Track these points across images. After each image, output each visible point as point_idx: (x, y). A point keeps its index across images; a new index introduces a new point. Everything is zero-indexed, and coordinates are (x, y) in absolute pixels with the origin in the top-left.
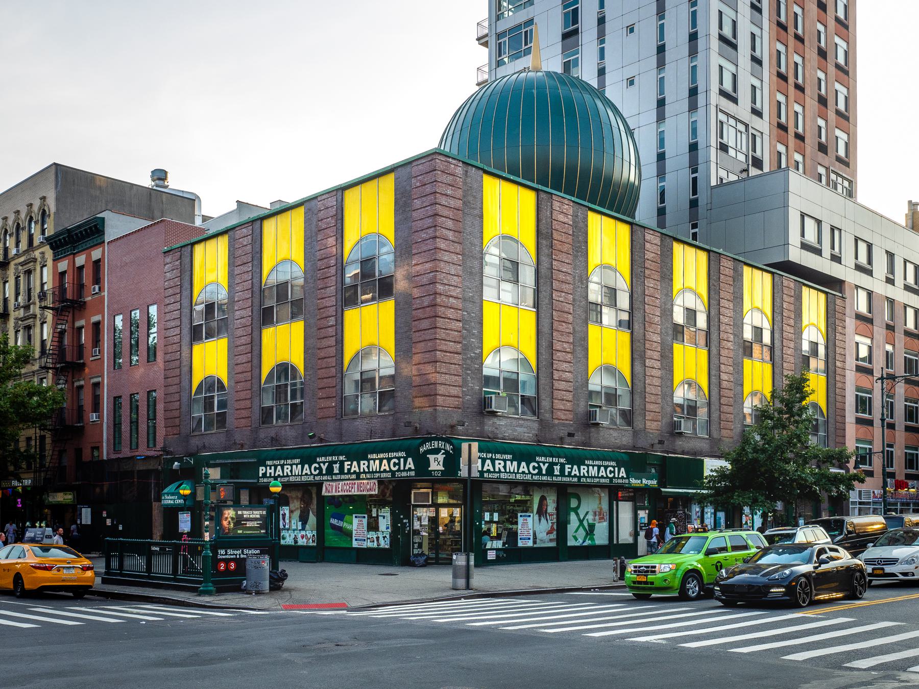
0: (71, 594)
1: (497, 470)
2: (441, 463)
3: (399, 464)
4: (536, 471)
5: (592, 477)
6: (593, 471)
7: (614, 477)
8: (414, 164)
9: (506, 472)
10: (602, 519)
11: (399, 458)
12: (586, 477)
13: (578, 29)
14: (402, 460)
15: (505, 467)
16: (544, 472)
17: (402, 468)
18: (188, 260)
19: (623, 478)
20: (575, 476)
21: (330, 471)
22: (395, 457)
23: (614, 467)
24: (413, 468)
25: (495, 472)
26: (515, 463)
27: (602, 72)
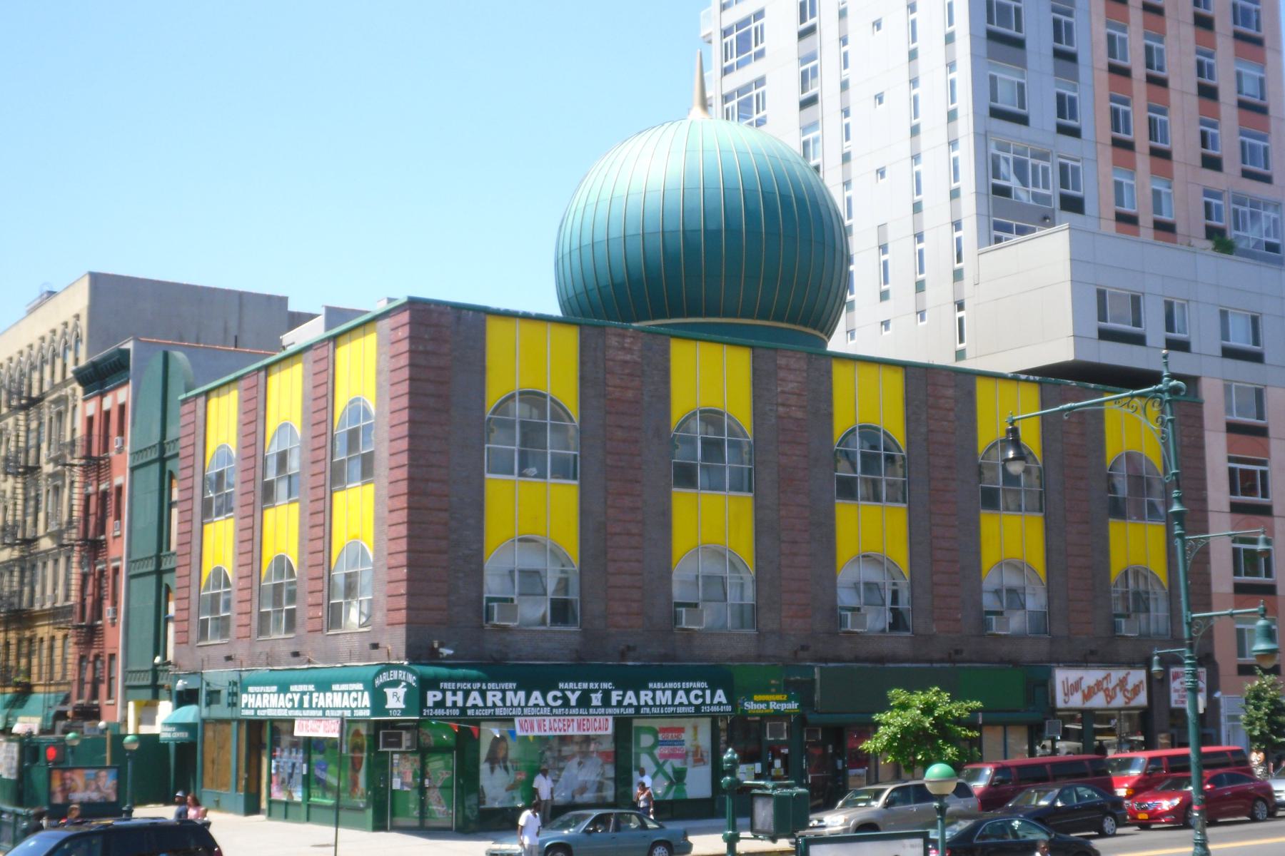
1: (489, 704)
2: (402, 699)
4: (559, 702)
5: (661, 706)
6: (664, 697)
7: (704, 703)
9: (505, 706)
10: (699, 760)
12: (651, 707)
15: (503, 700)
16: (573, 703)
18: (202, 431)
19: (720, 704)
20: (630, 705)
23: (703, 690)
25: (485, 707)
26: (522, 694)
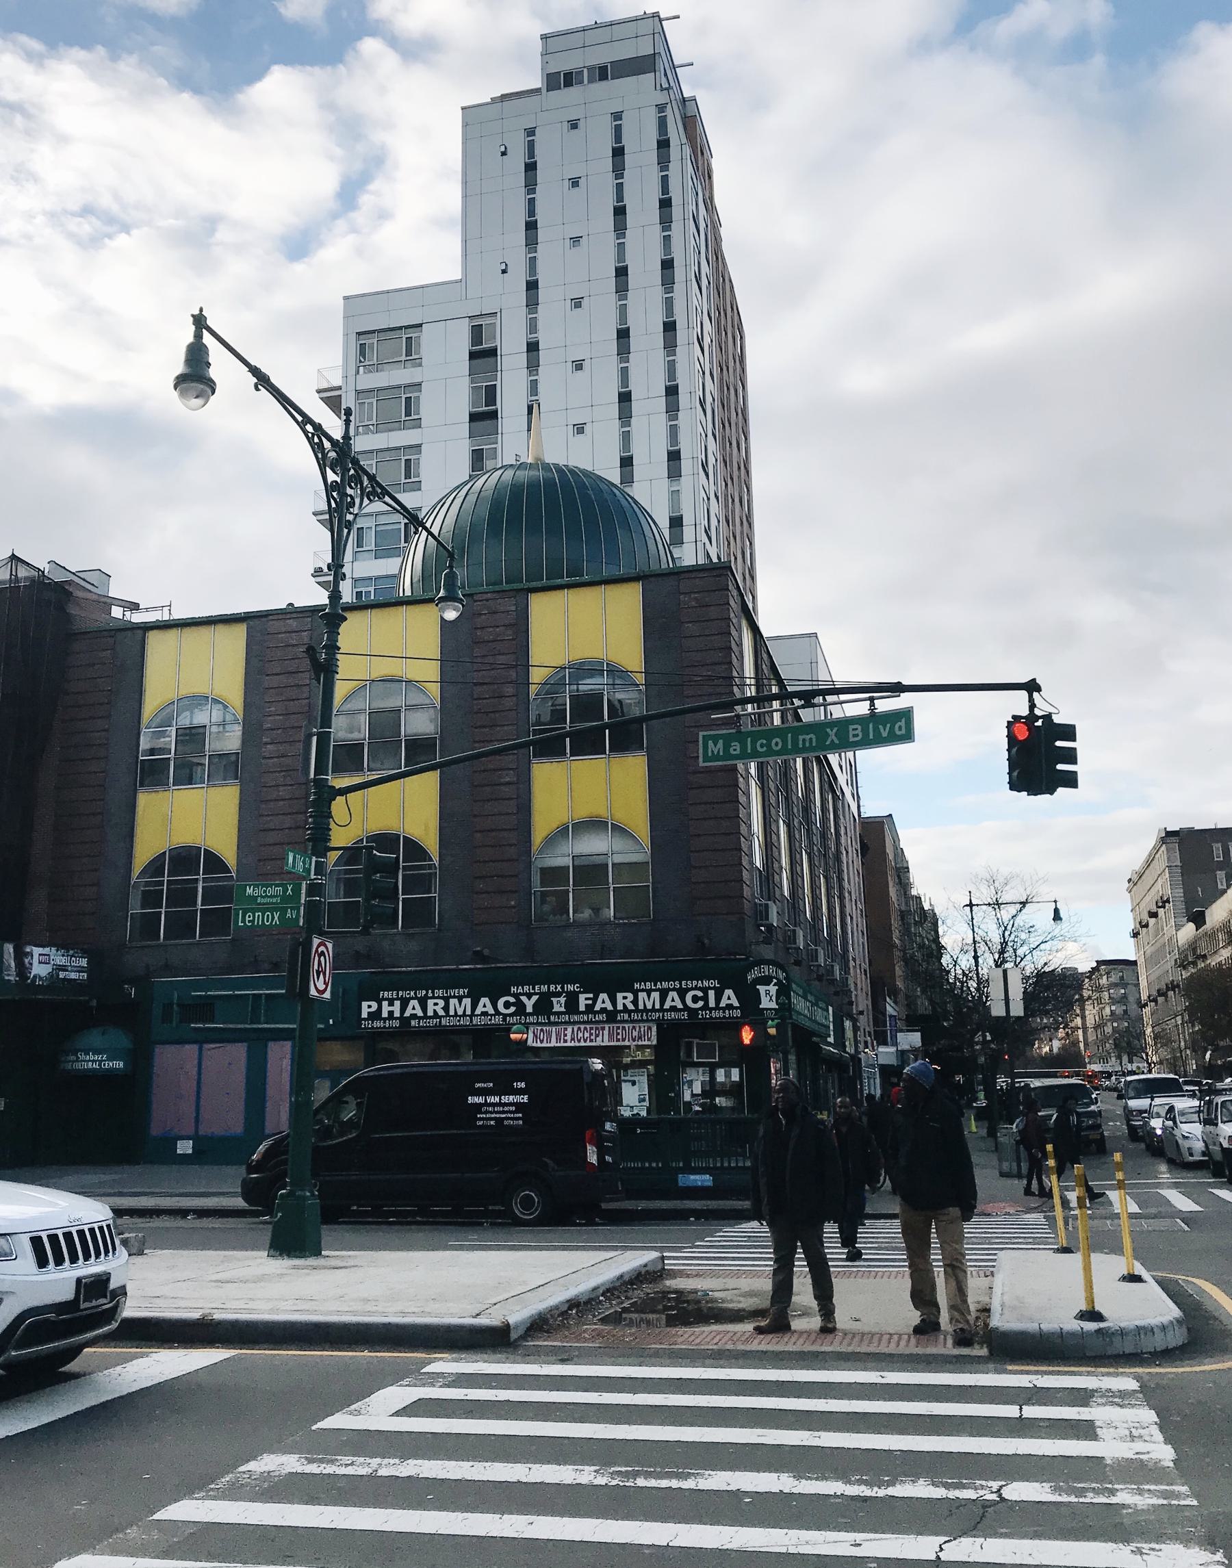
0: (746, 1204)
3: (705, 998)
8: (683, 576)
11: (705, 990)
13: (496, 411)
14: (711, 994)
16: (529, 1009)
17: (712, 1004)
21: (544, 1007)
22: (696, 988)
24: (736, 1004)
27: (627, 462)
